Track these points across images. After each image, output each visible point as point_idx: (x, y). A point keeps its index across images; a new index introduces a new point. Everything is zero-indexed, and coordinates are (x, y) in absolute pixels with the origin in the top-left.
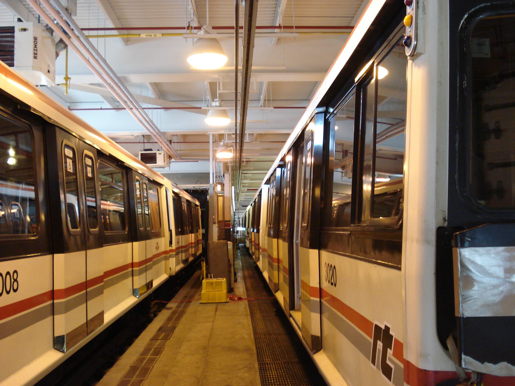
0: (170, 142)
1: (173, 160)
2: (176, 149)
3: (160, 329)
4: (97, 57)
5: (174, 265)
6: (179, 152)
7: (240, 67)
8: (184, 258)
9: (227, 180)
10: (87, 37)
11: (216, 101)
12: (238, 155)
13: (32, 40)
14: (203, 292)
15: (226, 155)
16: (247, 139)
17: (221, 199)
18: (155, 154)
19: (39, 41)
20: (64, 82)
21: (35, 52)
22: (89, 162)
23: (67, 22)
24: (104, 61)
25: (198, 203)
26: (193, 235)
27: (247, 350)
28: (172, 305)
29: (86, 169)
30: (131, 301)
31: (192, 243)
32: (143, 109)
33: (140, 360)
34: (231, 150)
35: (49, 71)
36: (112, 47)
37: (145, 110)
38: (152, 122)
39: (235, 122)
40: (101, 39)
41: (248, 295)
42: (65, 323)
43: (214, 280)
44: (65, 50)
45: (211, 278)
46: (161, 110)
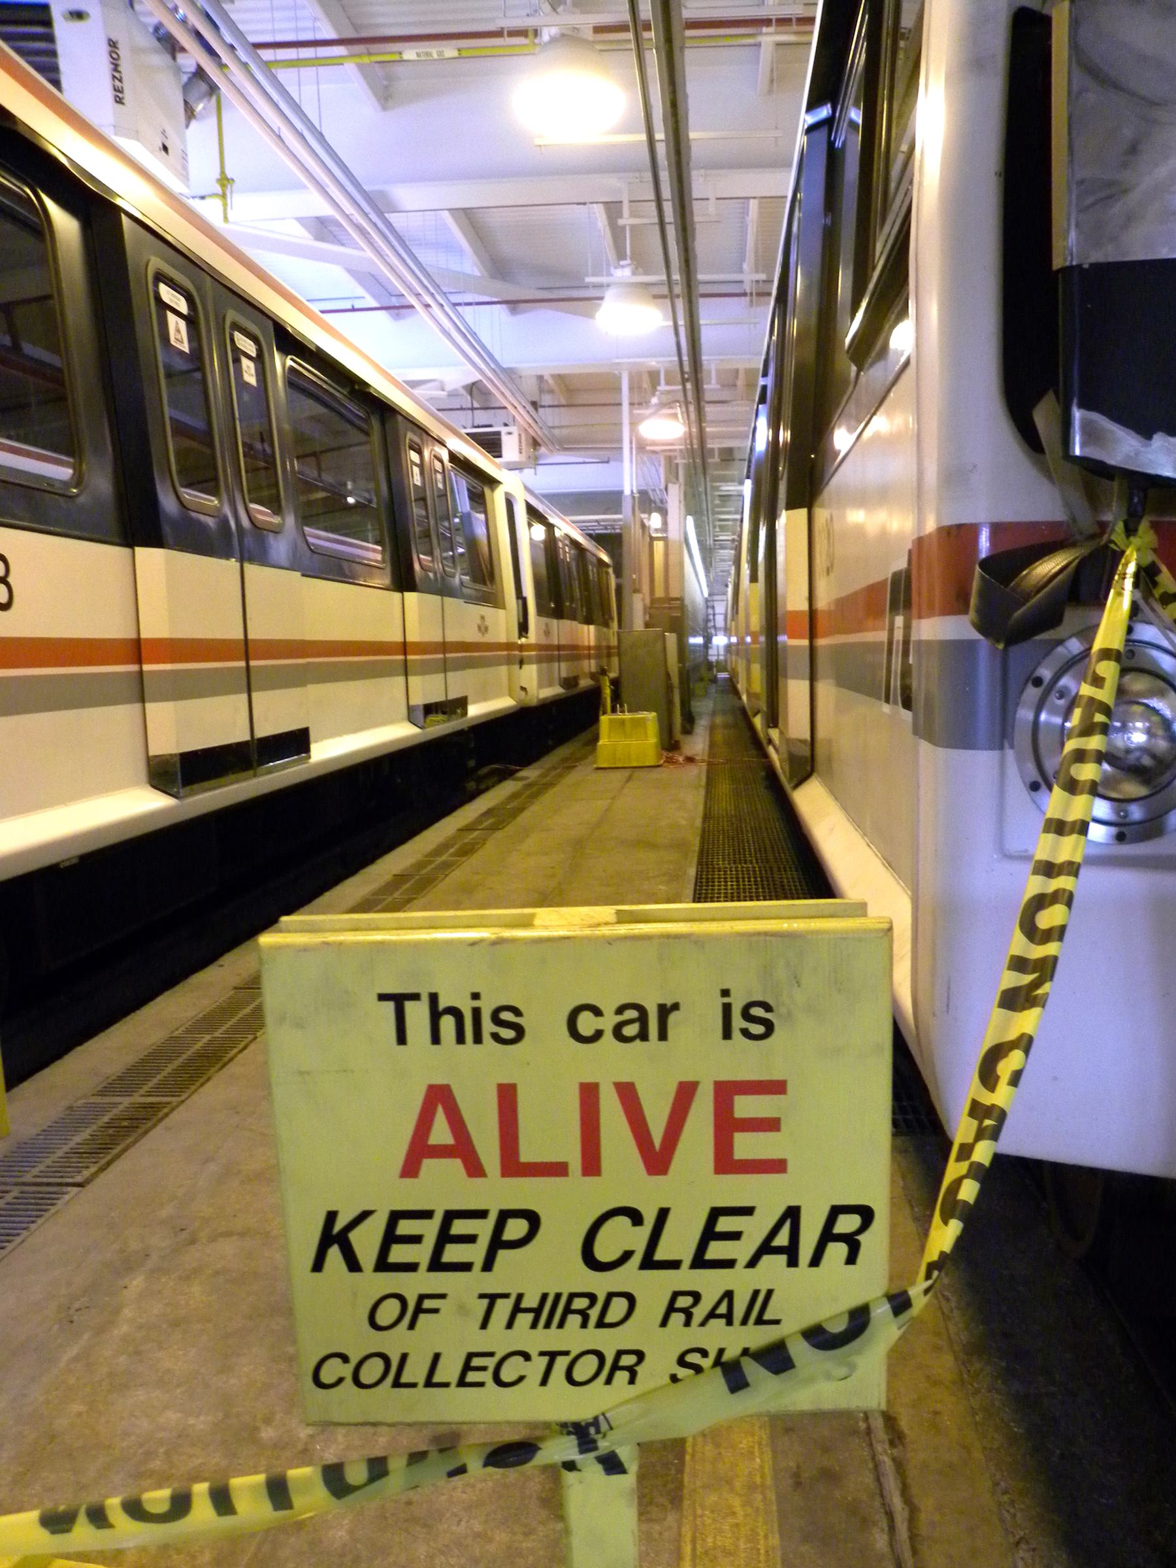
0: (534, 404)
1: (543, 450)
2: (550, 424)
3: (488, 813)
4: (299, 125)
5: (535, 684)
6: (556, 432)
7: (660, 135)
8: (564, 674)
9: (674, 499)
10: (266, 66)
11: (623, 267)
12: (694, 430)
13: (104, 49)
14: (601, 743)
15: (666, 428)
16: (711, 386)
17: (659, 546)
18: (499, 433)
19: (123, 51)
20: (219, 190)
21: (117, 83)
22: (246, 345)
23: (208, 16)
24: (320, 137)
25: (605, 558)
26: (592, 627)
27: (680, 846)
28: (530, 773)
29: (237, 361)
30: (397, 732)
31: (589, 648)
32: (456, 305)
33: (420, 865)
34: (675, 416)
35: (165, 149)
36: (337, 95)
37: (459, 308)
38: (474, 334)
39: (671, 323)
40: (308, 73)
41: (712, 754)
42: (181, 726)
43: (627, 716)
44: (214, 99)
45: (623, 712)
46: (498, 306)
